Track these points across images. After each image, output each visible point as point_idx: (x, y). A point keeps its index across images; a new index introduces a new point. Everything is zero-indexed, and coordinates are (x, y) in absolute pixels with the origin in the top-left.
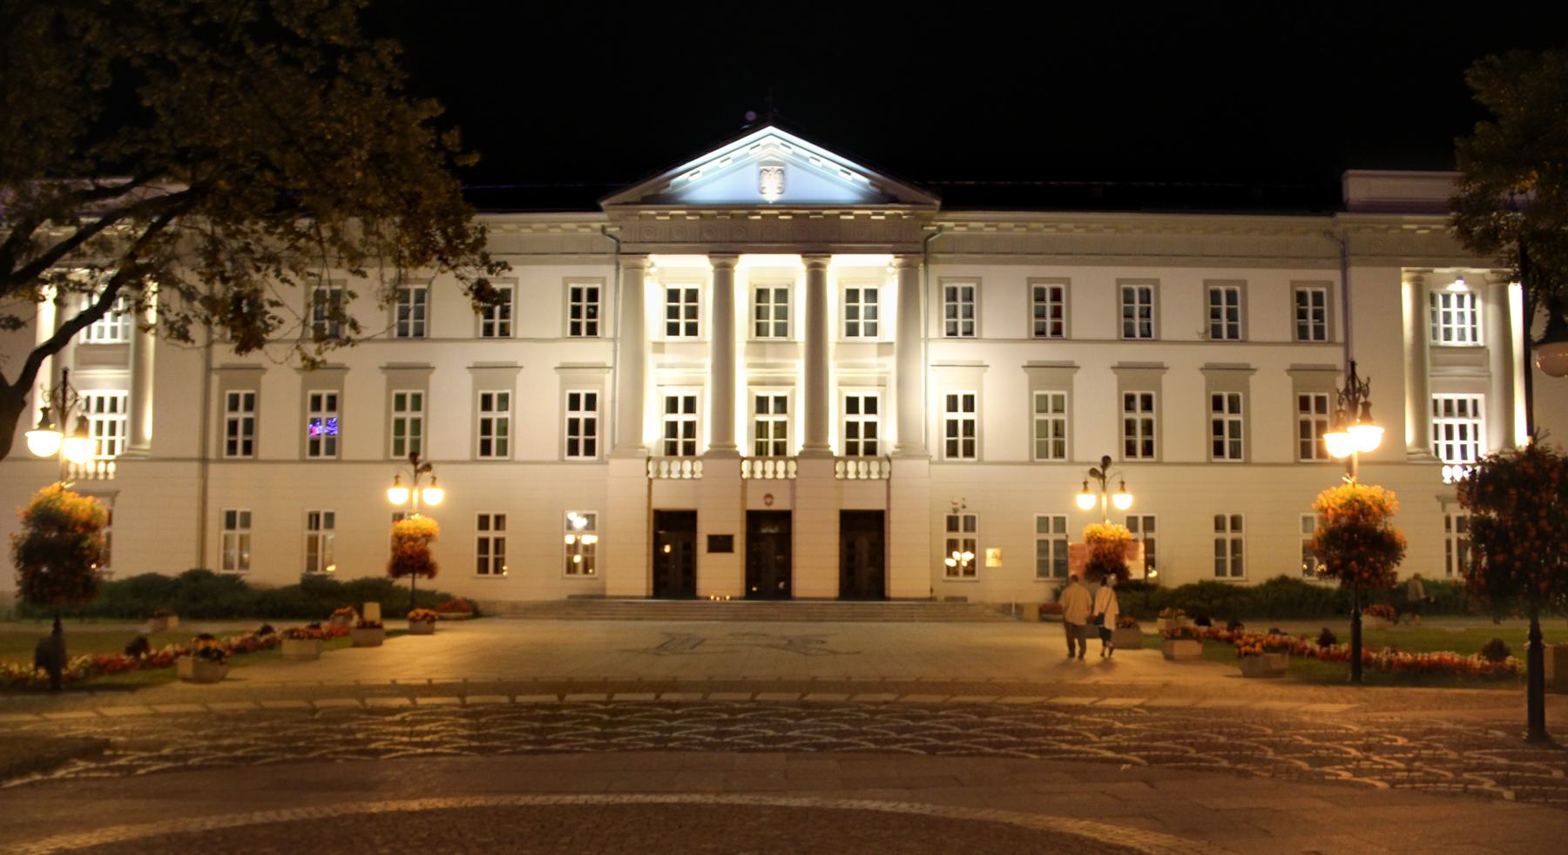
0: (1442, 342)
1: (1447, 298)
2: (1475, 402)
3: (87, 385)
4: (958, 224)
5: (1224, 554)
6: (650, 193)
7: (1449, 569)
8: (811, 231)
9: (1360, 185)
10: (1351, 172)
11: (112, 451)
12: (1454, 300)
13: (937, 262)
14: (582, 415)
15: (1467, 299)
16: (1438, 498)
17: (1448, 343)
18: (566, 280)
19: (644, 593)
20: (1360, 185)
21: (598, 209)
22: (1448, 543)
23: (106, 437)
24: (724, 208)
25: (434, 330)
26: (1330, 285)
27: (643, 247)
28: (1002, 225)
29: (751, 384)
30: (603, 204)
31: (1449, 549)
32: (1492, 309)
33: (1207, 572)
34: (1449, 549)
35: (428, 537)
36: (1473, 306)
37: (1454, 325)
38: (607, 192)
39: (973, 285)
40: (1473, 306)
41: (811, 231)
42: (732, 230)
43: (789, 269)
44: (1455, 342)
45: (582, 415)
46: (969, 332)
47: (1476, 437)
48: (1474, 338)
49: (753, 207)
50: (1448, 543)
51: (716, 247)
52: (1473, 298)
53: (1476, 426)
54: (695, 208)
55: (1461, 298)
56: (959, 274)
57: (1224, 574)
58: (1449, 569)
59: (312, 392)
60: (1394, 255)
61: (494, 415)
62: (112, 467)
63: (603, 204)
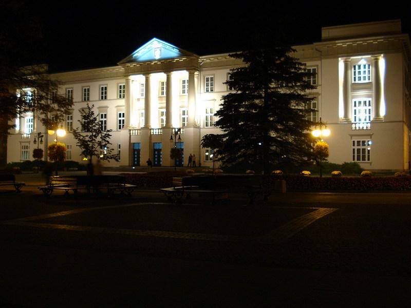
0: (357, 81)
1: (359, 67)
2: (369, 101)
3: (353, 97)
4: (203, 59)
5: (360, 153)
6: (128, 60)
7: (354, 159)
8: (167, 66)
9: (326, 32)
10: (323, 28)
11: (370, 120)
12: (362, 67)
13: (203, 71)
14: (122, 119)
15: (367, 66)
16: (350, 135)
17: (360, 82)
18: (118, 84)
19: (128, 165)
20: (326, 32)
21: (118, 65)
22: (354, 150)
23: (368, 115)
24: (144, 62)
25: (108, 98)
26: (317, 66)
27: (149, 72)
28: (219, 58)
29: (180, 107)
30: (118, 64)
31: (354, 153)
32: (374, 69)
33: (350, 160)
34: (354, 153)
35: (326, 148)
36: (369, 68)
37: (362, 75)
38: (119, 60)
39: (316, 68)
40: (369, 68)
41: (167, 66)
42: (148, 68)
43: (162, 76)
44: (362, 81)
45: (122, 119)
46: (212, 91)
47: (370, 113)
48: (369, 79)
49: (151, 61)
50: (354, 150)
51: (144, 72)
52: (369, 66)
53: (370, 110)
54: (139, 62)
55: (365, 66)
56: (208, 74)
57: (360, 160)
58: (354, 159)
59: (119, 113)
60: (336, 54)
61: (186, 116)
62: (369, 125)
63: (118, 64)
